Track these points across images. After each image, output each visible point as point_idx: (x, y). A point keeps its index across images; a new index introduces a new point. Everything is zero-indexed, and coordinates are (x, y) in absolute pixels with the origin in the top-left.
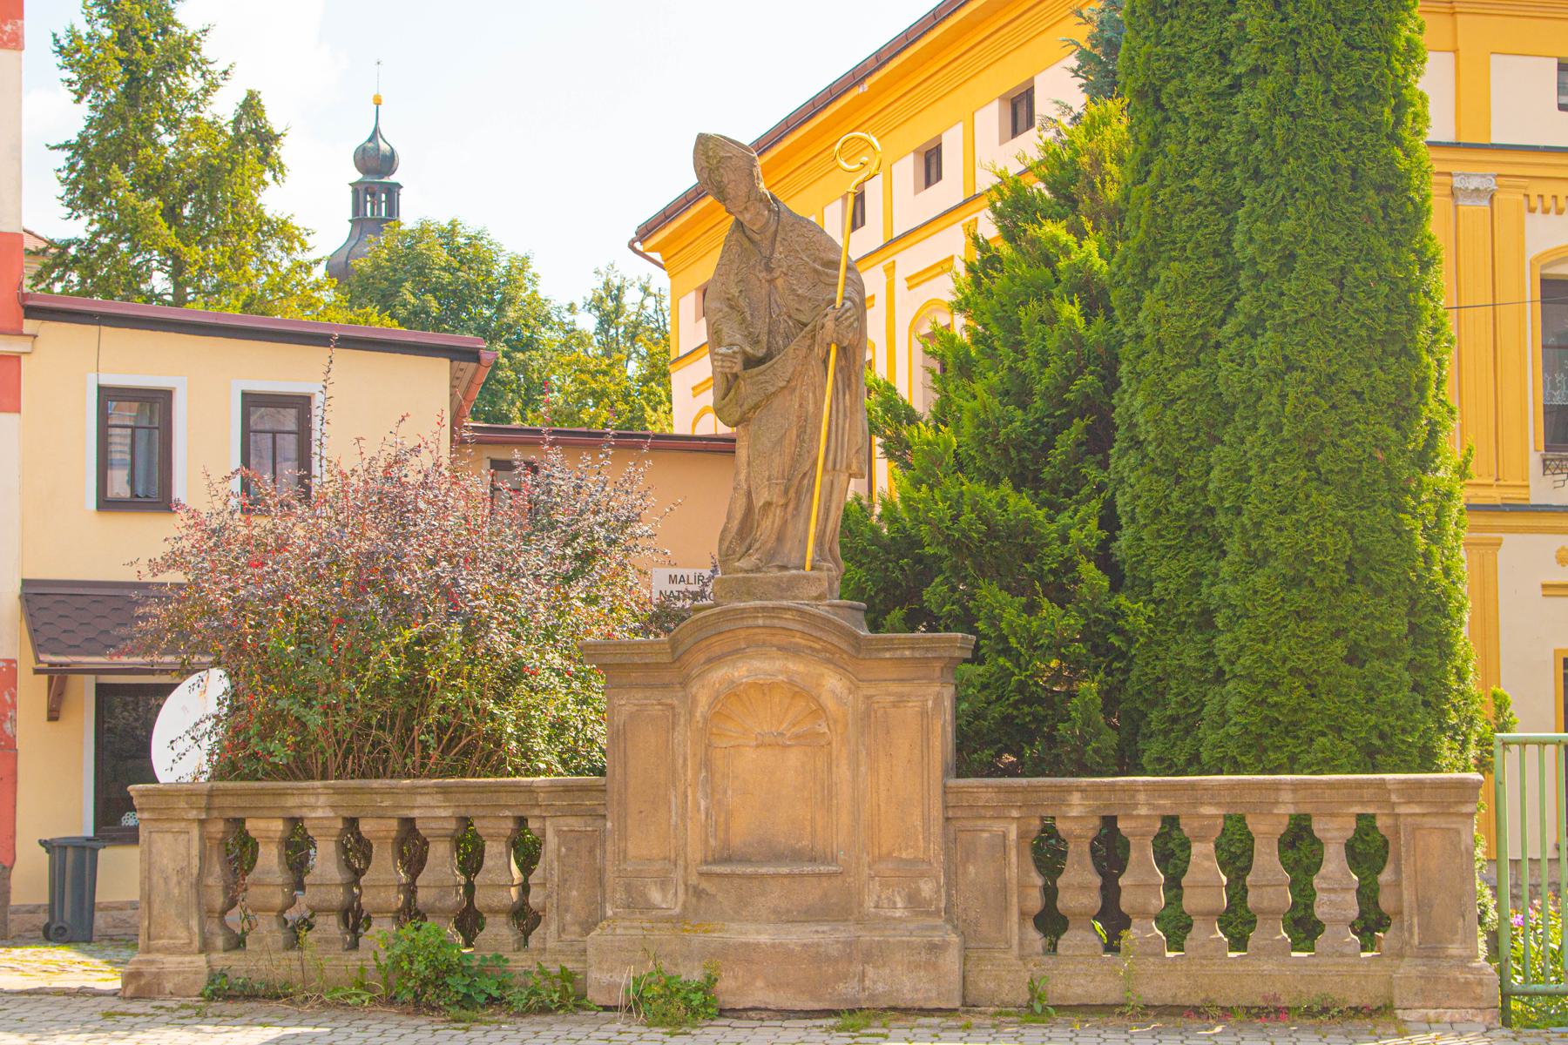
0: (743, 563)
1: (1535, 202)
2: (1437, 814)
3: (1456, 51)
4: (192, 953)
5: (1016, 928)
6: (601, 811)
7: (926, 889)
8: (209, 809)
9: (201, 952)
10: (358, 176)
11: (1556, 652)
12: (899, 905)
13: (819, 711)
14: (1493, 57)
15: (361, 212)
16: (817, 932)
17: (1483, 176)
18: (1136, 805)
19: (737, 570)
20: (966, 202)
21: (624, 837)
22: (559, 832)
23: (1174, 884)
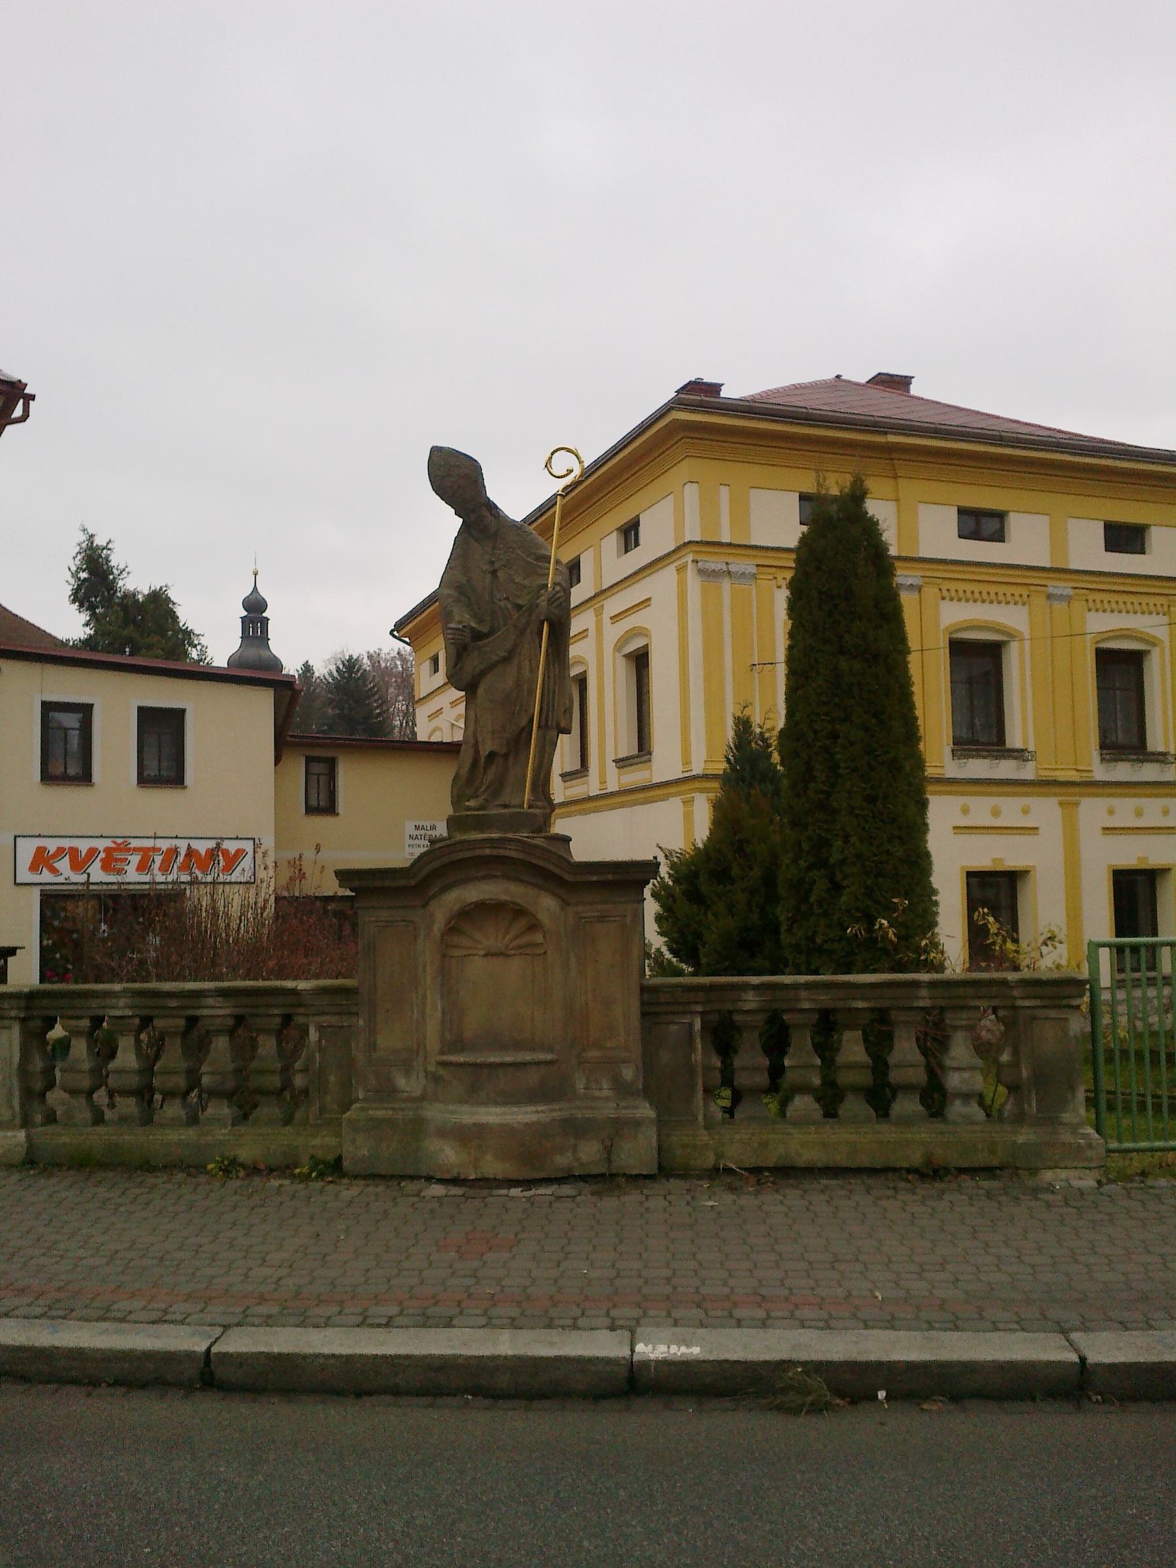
0: (472, 803)
1: (945, 593)
2: (1045, 1007)
3: (897, 500)
4: (13, 1129)
5: (701, 1103)
6: (354, 1009)
7: (628, 1073)
8: (28, 1008)
9: (22, 1127)
10: (245, 613)
11: (962, 868)
12: (605, 1086)
13: (535, 926)
14: (920, 504)
15: (247, 633)
16: (537, 1112)
17: (916, 577)
18: (798, 1000)
19: (469, 809)
20: (596, 596)
21: (372, 1029)
22: (320, 1028)
23: (829, 1063)
